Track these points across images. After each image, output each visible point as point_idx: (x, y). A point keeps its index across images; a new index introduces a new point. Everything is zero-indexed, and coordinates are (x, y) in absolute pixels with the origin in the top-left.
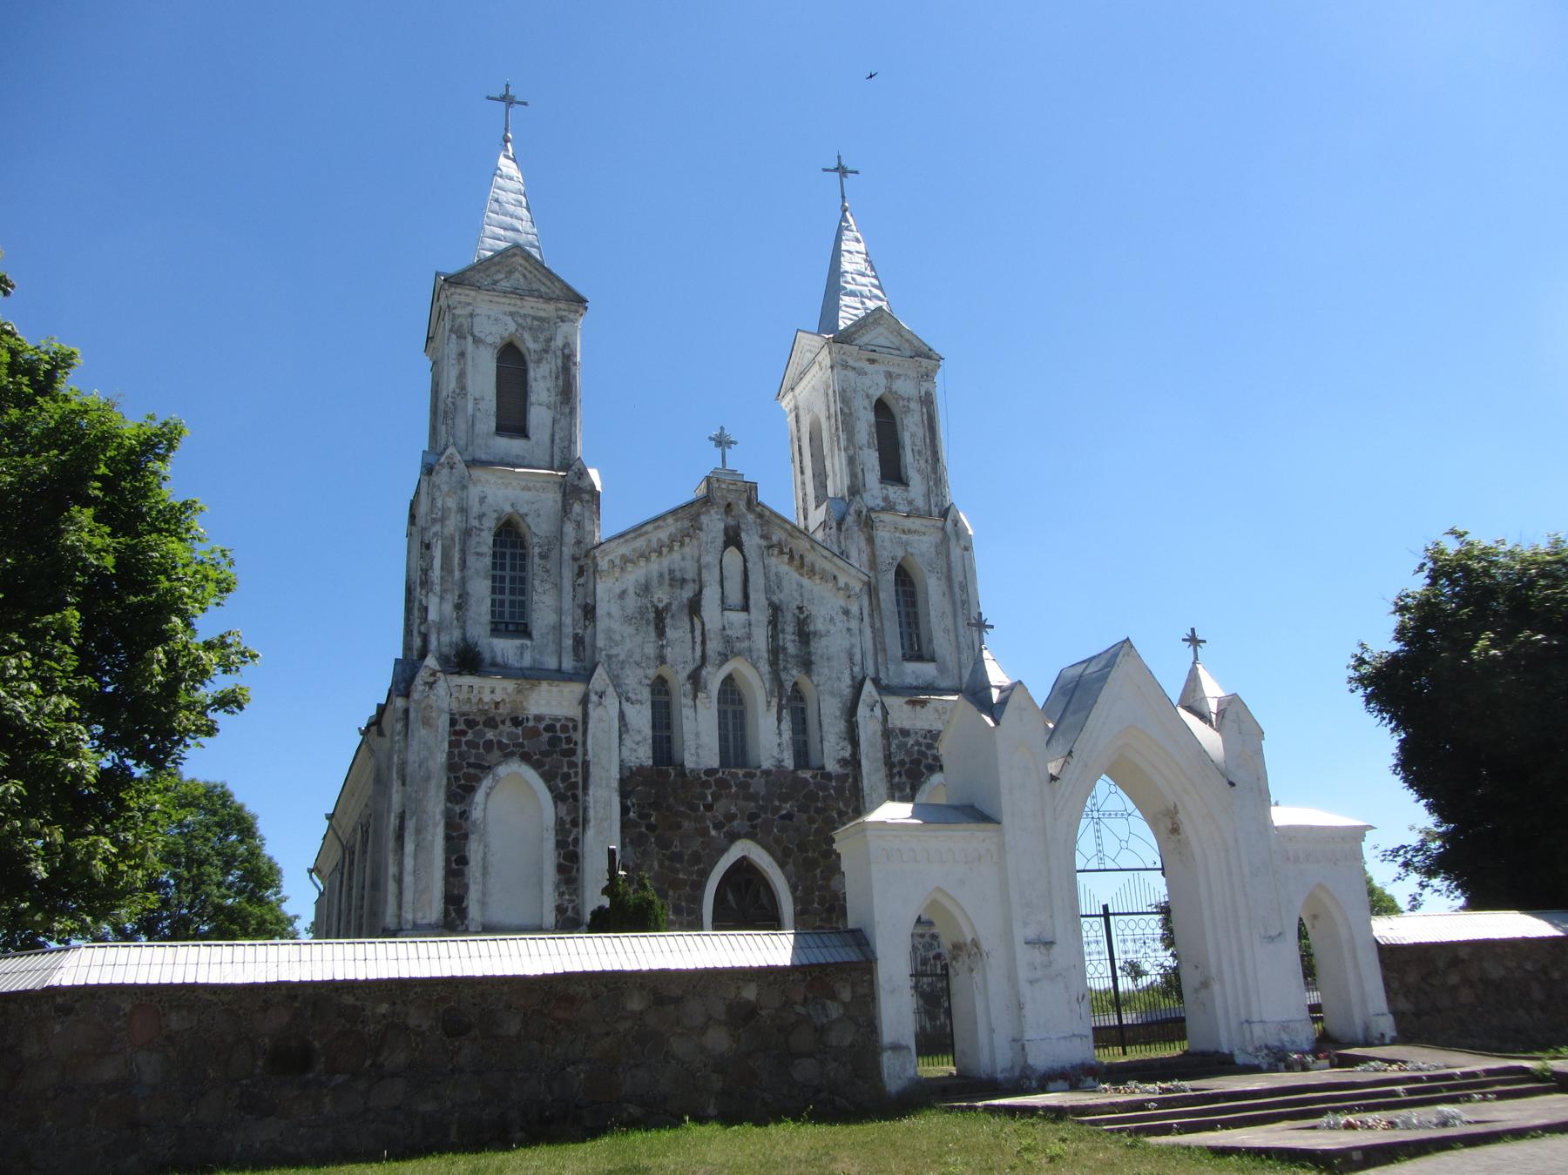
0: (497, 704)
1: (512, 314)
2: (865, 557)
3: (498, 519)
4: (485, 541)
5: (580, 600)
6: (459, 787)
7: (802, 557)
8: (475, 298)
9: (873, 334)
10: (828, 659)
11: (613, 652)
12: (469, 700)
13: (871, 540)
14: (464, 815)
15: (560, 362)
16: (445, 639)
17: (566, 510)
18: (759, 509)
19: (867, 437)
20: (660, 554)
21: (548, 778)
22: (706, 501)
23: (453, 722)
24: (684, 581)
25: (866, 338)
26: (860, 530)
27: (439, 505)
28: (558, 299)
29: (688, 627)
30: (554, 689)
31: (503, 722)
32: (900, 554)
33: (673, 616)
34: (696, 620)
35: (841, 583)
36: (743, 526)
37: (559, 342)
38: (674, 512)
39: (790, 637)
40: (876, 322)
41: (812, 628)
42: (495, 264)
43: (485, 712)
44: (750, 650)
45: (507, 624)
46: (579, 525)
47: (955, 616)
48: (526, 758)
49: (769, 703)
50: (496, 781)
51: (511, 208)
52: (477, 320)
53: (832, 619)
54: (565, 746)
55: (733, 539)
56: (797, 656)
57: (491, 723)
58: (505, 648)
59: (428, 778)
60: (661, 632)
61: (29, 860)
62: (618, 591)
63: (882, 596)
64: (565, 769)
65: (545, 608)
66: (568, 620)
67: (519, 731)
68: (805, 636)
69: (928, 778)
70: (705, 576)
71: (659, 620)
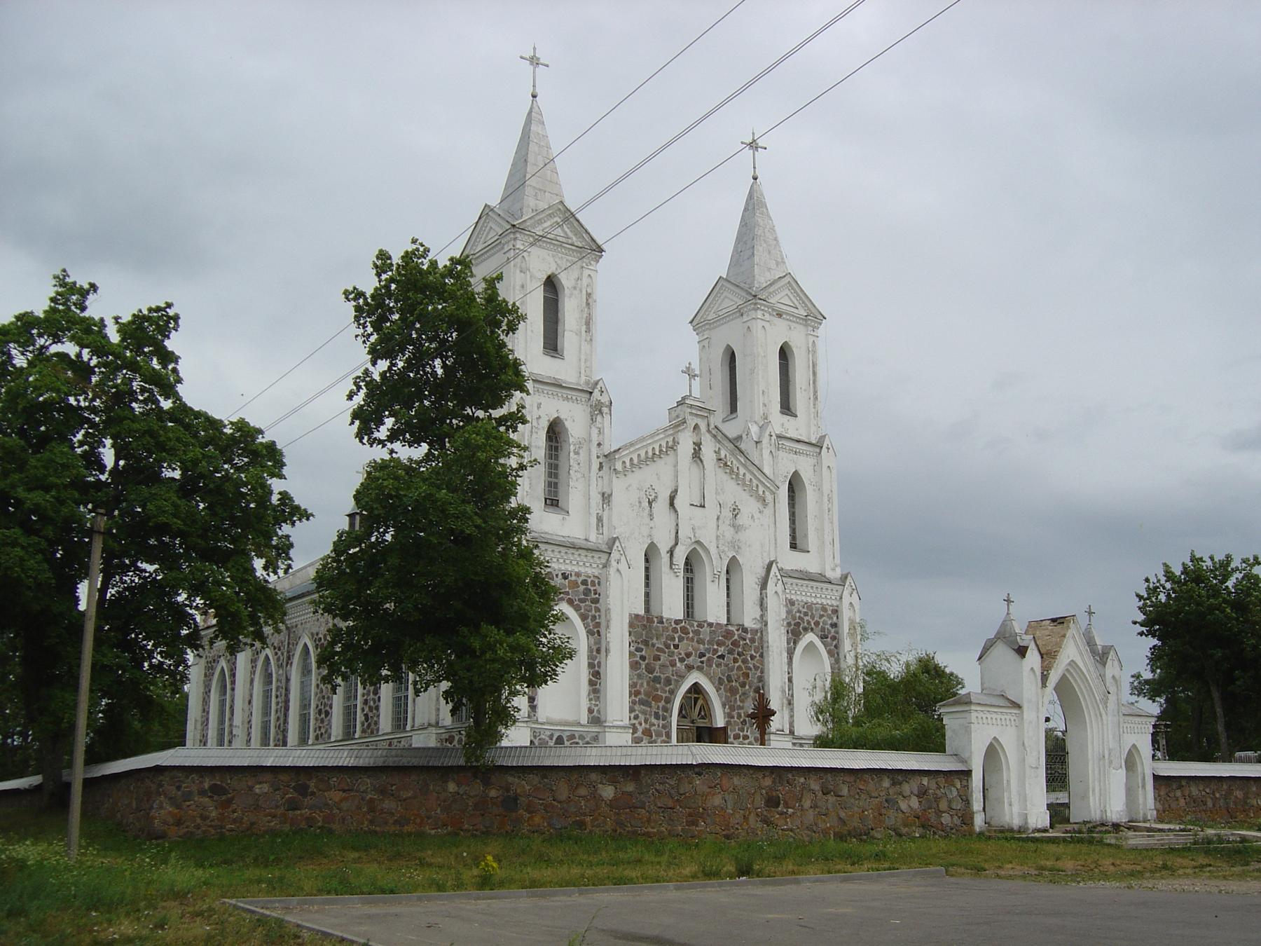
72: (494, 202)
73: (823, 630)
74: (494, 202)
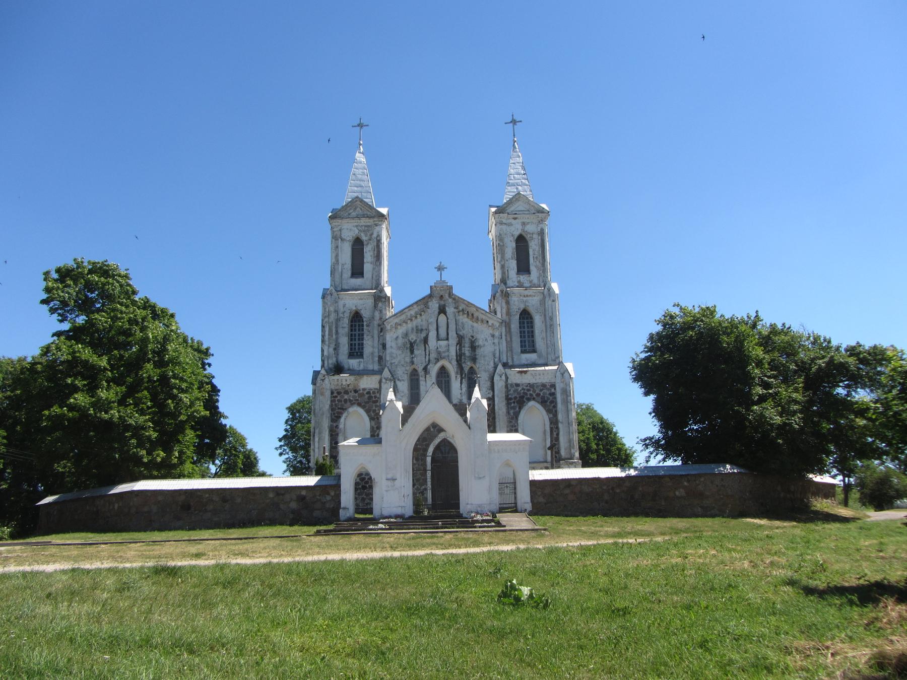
0: (348, 385)
1: (357, 226)
2: (504, 311)
3: (350, 313)
4: (345, 322)
5: (381, 342)
6: (335, 417)
7: (472, 315)
8: (341, 222)
9: (516, 206)
10: (484, 357)
11: (393, 362)
12: (338, 385)
13: (508, 303)
14: (337, 427)
15: (375, 244)
16: (330, 362)
17: (375, 306)
18: (453, 297)
19: (511, 255)
20: (411, 320)
21: (368, 412)
22: (430, 296)
23: (332, 393)
24: (422, 330)
25: (512, 209)
26: (503, 298)
27: (327, 310)
28: (373, 217)
29: (423, 348)
30: (369, 378)
31: (351, 392)
32: (522, 307)
33: (417, 345)
34: (426, 345)
35: (490, 323)
36: (447, 304)
37: (375, 235)
38: (416, 303)
39: (467, 349)
40: (517, 200)
41: (477, 344)
42: (349, 207)
43: (344, 388)
44: (448, 356)
45: (357, 353)
46: (381, 311)
47: (546, 332)
48: (359, 405)
49: (456, 377)
50: (348, 414)
51: (360, 177)
52: (343, 231)
53: (486, 340)
54: (374, 399)
55: (442, 310)
56: (470, 357)
57: (346, 392)
58: (354, 363)
59: (323, 414)
60: (412, 352)
61: (143, 458)
62: (395, 337)
63: (513, 326)
64: (374, 408)
65: (370, 346)
66: (376, 350)
67: (357, 395)
68: (473, 348)
69: (527, 403)
70: (430, 327)
71: (412, 347)
72: (328, 285)
73: (543, 398)
74: (328, 285)
